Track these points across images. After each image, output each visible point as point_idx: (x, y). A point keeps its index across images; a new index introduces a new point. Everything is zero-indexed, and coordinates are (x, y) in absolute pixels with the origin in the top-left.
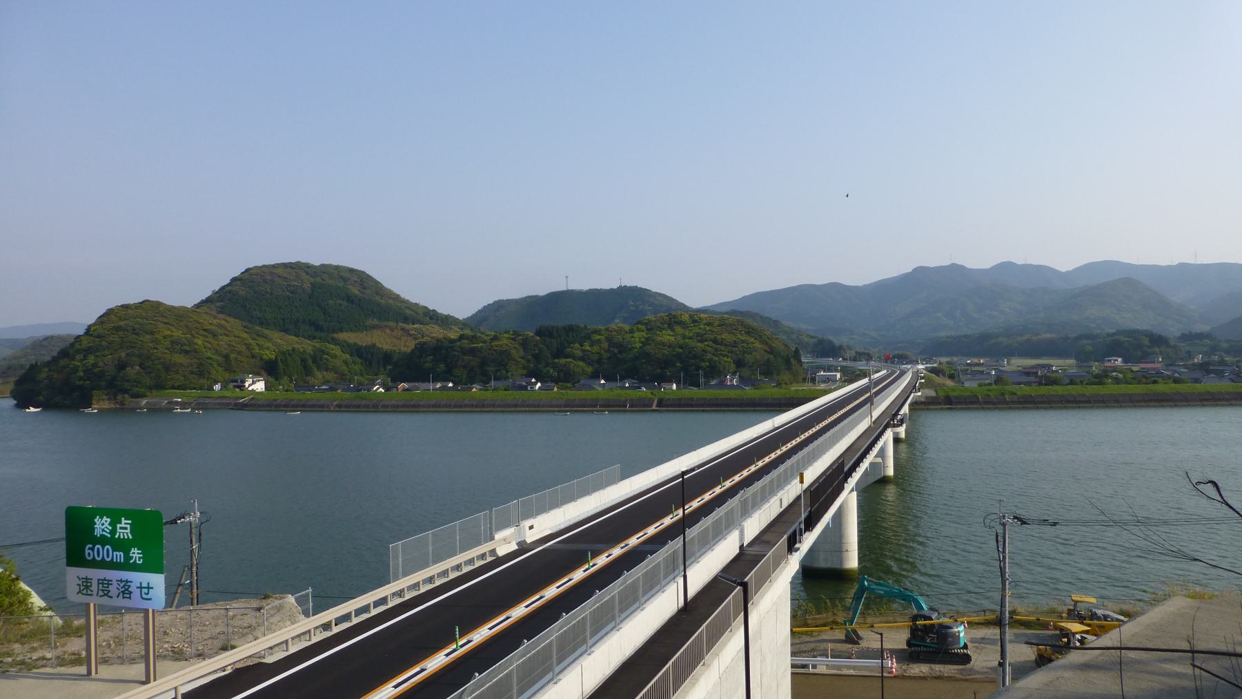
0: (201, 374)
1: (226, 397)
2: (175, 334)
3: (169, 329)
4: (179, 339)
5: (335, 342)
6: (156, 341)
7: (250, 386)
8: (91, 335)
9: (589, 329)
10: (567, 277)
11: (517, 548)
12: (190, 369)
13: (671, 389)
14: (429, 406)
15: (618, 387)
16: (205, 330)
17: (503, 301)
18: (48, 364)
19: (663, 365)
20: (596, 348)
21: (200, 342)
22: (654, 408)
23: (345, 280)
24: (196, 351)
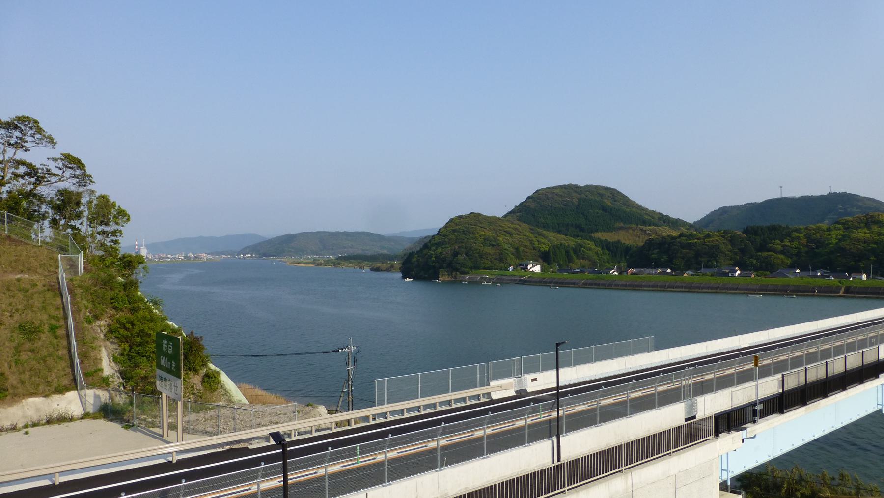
0: (501, 260)
1: (515, 276)
2: (487, 234)
3: (484, 231)
4: (489, 237)
5: (592, 239)
6: (476, 239)
7: (531, 268)
8: (440, 235)
9: (790, 228)
10: (781, 187)
11: (515, 394)
12: (494, 257)
13: (861, 279)
14: (649, 286)
15: (809, 276)
16: (505, 231)
17: (727, 207)
18: (418, 252)
19: (857, 258)
20: (795, 244)
21: (501, 239)
22: (841, 294)
23: (601, 195)
24: (499, 245)
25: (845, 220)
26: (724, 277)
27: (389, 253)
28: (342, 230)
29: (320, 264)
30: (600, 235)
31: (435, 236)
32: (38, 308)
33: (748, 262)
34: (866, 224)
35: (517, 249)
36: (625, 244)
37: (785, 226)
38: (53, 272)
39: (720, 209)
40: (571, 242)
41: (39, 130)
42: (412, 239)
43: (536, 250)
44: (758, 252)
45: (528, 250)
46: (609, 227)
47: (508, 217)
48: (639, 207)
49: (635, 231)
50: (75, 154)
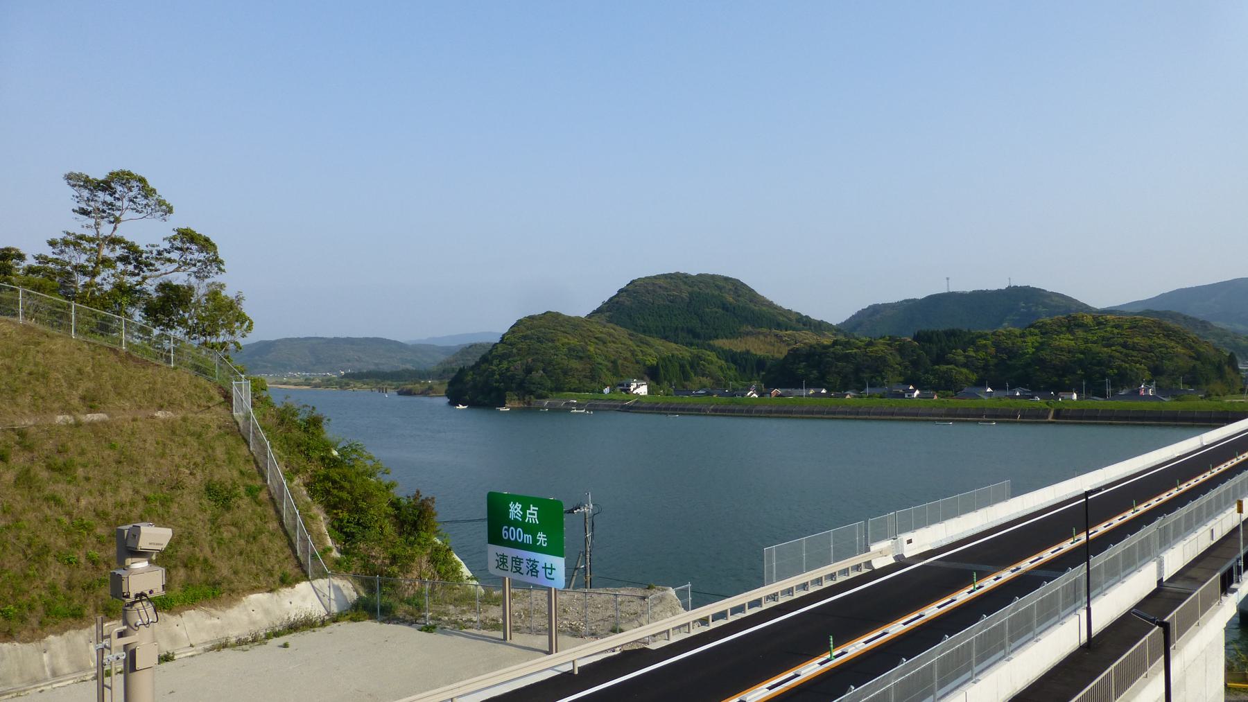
0: (593, 379)
1: (615, 400)
2: (572, 342)
3: (566, 337)
5: (712, 348)
6: (556, 348)
7: (634, 389)
8: (505, 343)
10: (948, 279)
11: (894, 561)
14: (802, 412)
16: (596, 338)
17: (878, 305)
18: (472, 368)
19: (1061, 372)
20: (981, 354)
21: (592, 349)
22: (1050, 419)
23: (720, 288)
24: (589, 357)
25: (1042, 322)
26: (899, 399)
27: (414, 369)
28: (344, 336)
29: (316, 386)
30: (721, 343)
31: (498, 345)
32: (224, 462)
33: (923, 378)
34: (1068, 328)
35: (614, 362)
36: (756, 355)
37: (967, 331)
38: (204, 406)
39: (870, 307)
40: (685, 352)
41: (148, 192)
42: (446, 350)
43: (639, 363)
44: (934, 364)
45: (628, 364)
46: (732, 331)
47: (594, 318)
48: (770, 304)
49: (767, 337)
50: (199, 229)
